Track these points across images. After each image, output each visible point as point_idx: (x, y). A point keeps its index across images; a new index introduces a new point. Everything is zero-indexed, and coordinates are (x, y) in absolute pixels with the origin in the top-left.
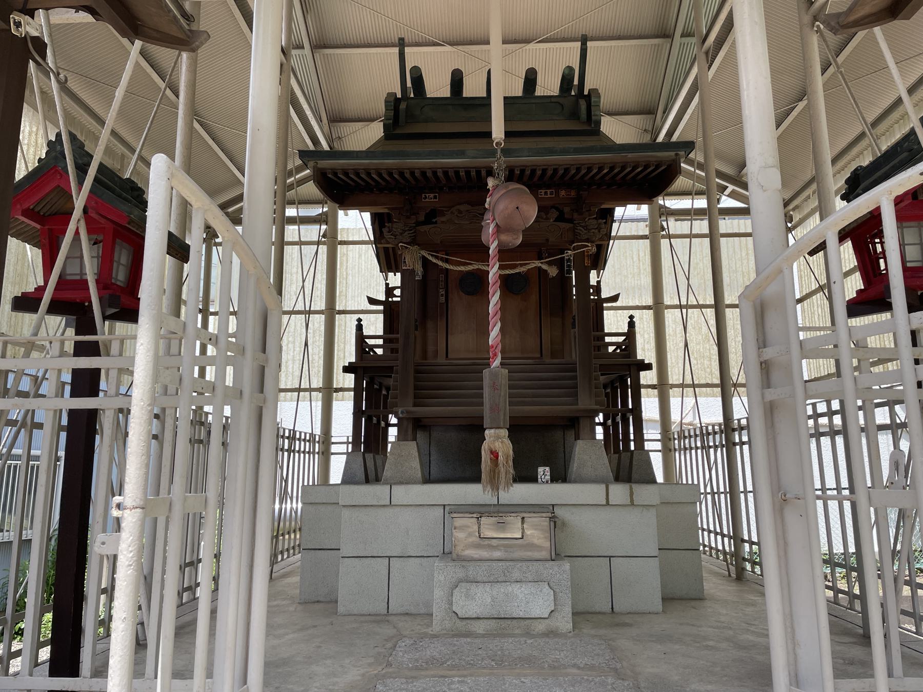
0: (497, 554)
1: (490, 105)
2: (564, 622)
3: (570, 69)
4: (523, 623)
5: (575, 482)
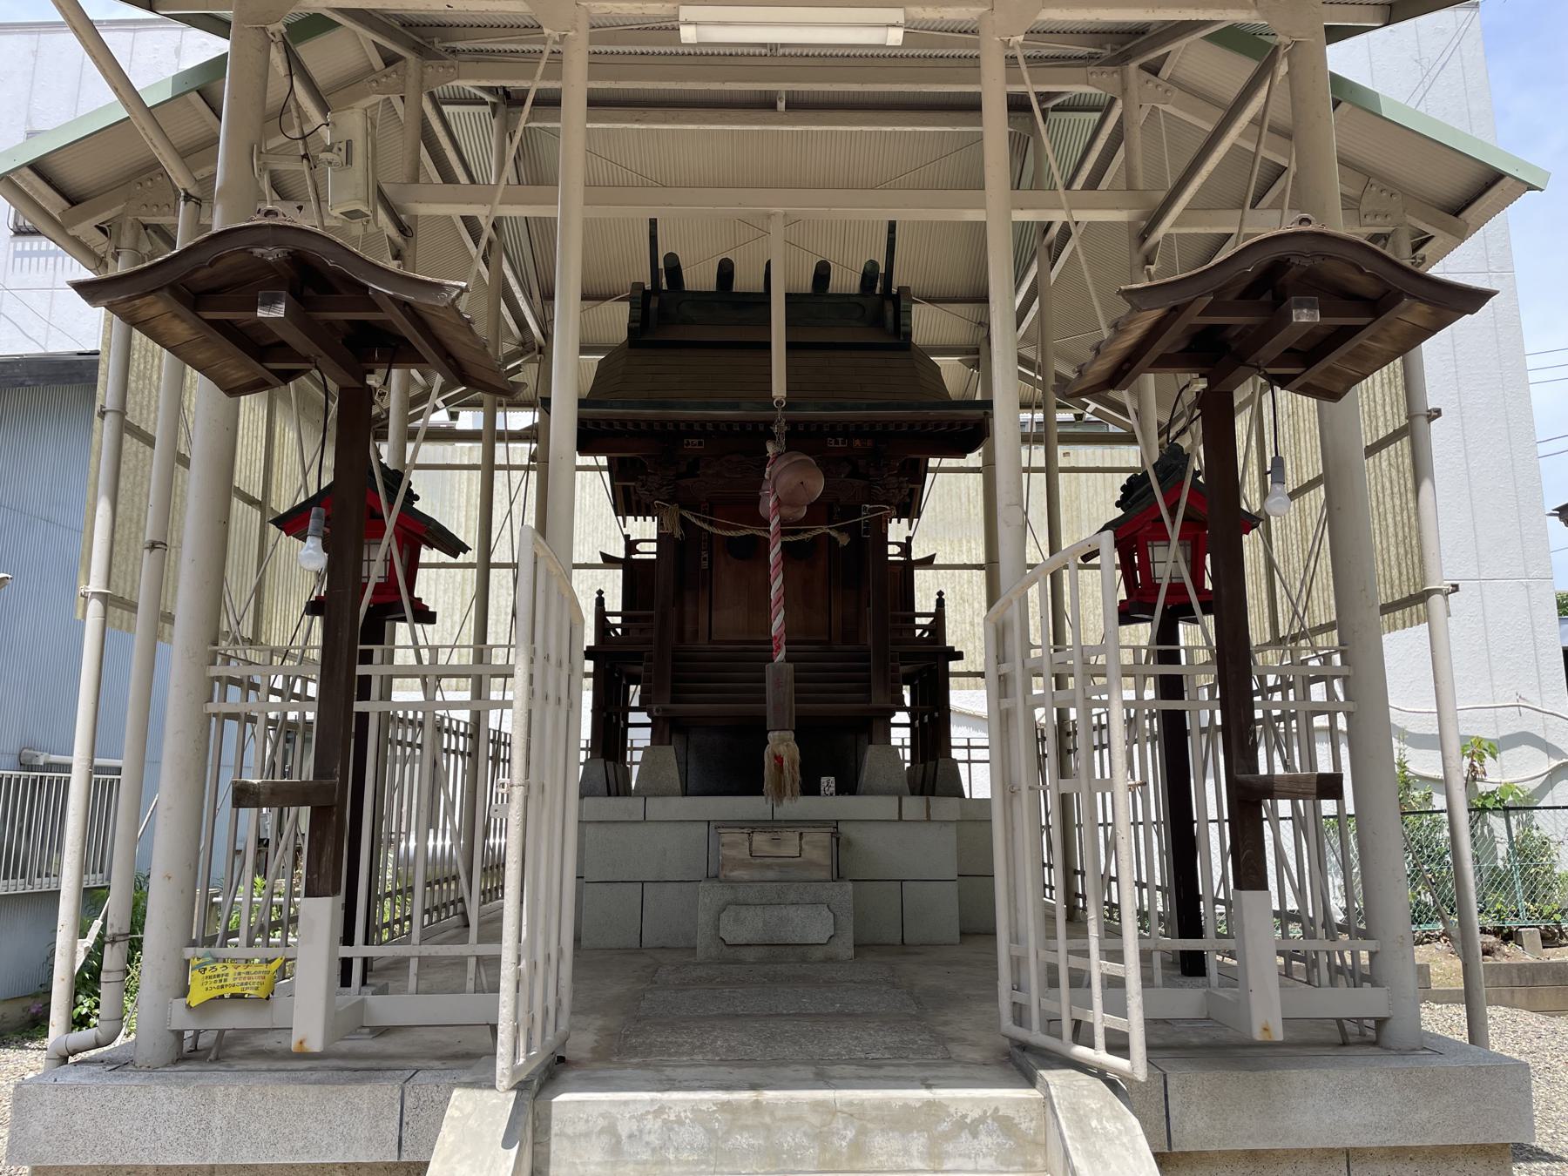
0: (770, 875)
1: (769, 304)
2: (845, 948)
3: (873, 264)
4: (799, 950)
5: (864, 794)
